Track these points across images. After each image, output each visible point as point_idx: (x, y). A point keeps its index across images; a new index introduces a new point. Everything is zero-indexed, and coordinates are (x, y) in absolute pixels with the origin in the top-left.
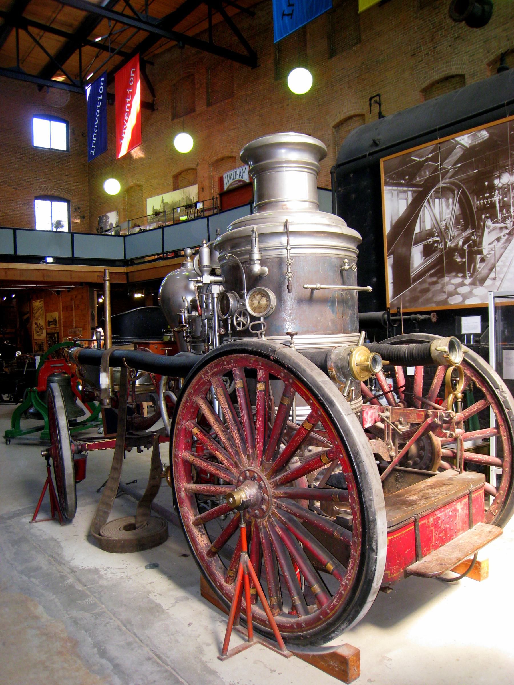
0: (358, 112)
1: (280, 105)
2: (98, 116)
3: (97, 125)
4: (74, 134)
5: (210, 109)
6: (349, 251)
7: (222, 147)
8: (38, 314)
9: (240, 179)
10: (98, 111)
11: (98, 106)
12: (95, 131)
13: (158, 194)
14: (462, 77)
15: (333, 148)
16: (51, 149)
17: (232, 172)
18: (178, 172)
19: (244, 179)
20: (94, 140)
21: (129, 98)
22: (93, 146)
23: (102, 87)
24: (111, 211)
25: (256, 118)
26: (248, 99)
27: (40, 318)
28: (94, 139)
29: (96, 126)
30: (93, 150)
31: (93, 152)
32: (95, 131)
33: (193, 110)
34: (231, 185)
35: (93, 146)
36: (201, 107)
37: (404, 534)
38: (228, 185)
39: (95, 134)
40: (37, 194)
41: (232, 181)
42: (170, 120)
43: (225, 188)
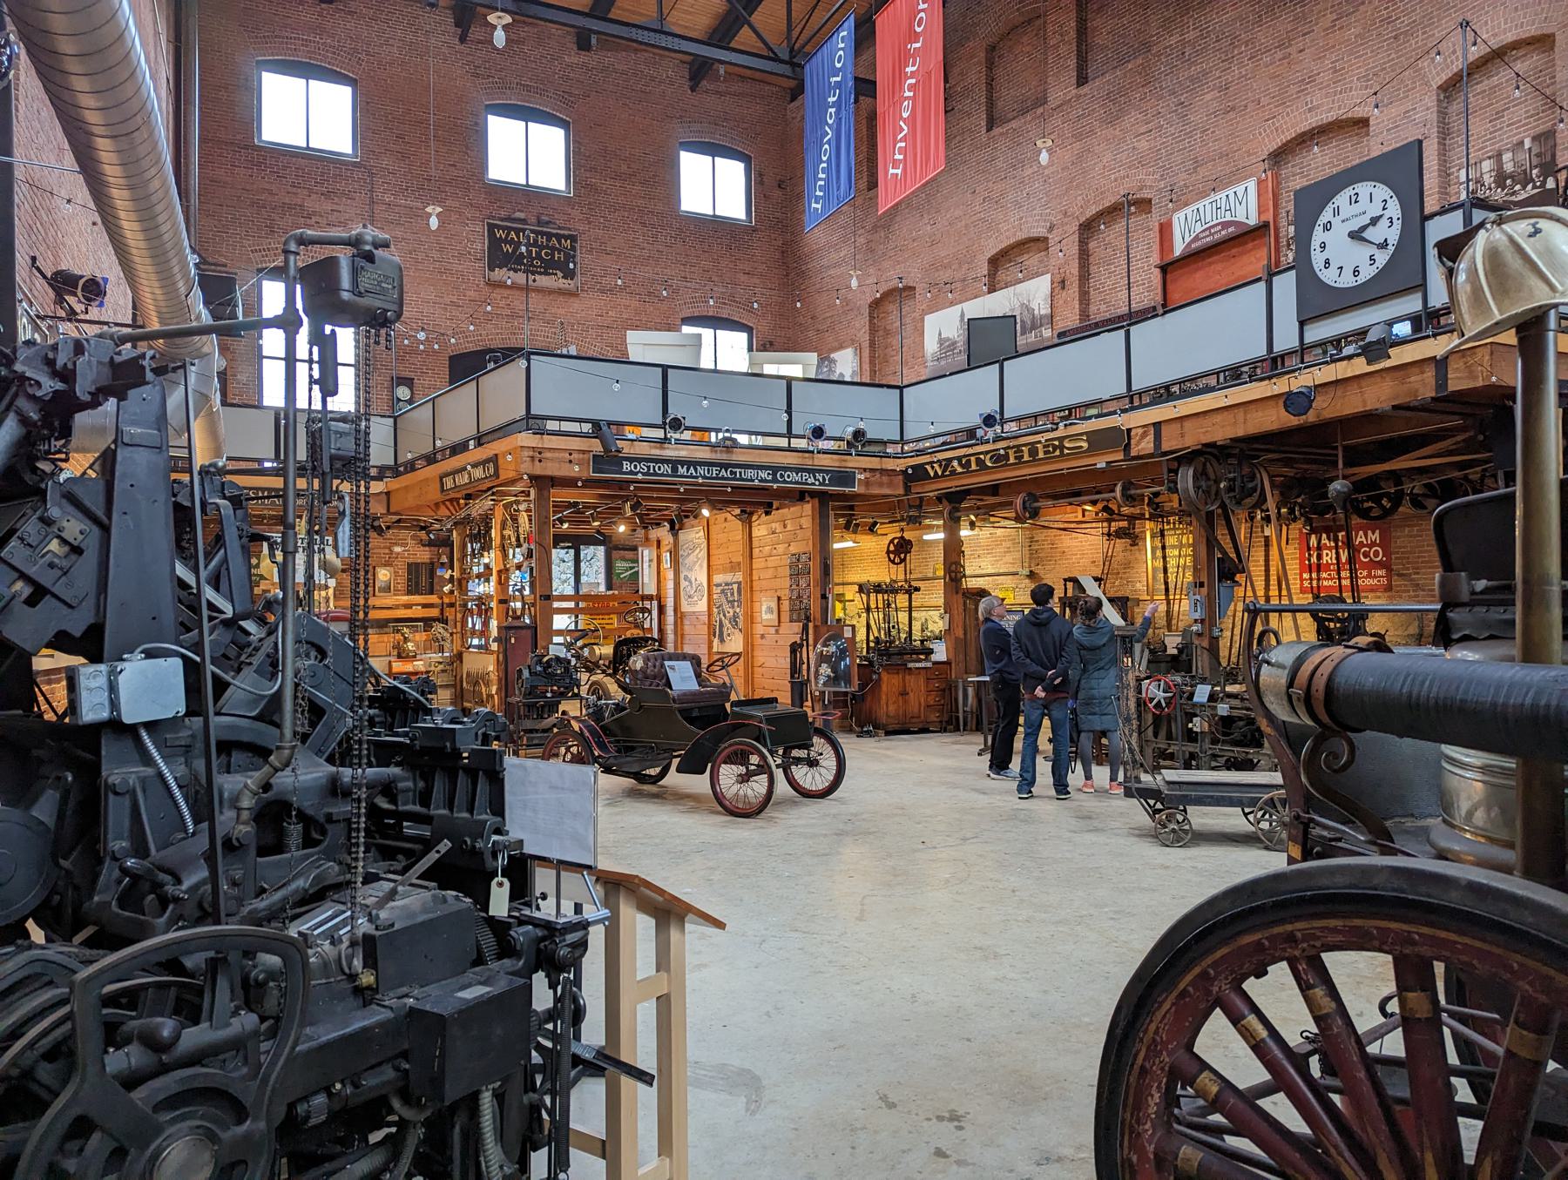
0: (1532, 30)
1: (1279, 55)
2: (830, 122)
3: (829, 142)
4: (760, 182)
5: (1085, 89)
6: (99, 606)
7: (1116, 180)
8: (692, 558)
9: (1228, 218)
10: (832, 110)
11: (831, 100)
12: (824, 159)
13: (952, 304)
14: (1363, 123)
15: (1439, 143)
16: (714, 216)
17: (1201, 206)
18: (1001, 251)
19: (1241, 218)
20: (821, 179)
21: (913, 65)
22: (819, 193)
23: (841, 52)
24: (841, 347)
25: (1208, 97)
26: (1188, 51)
27: (697, 567)
28: (821, 176)
29: (827, 146)
30: (817, 202)
31: (819, 206)
32: (824, 159)
33: (1042, 101)
34: (1196, 239)
35: (819, 193)
36: (1061, 88)
37: (1518, 1012)
38: (1187, 240)
39: (825, 165)
40: (687, 313)
41: (1199, 228)
42: (984, 130)
43: (1179, 249)
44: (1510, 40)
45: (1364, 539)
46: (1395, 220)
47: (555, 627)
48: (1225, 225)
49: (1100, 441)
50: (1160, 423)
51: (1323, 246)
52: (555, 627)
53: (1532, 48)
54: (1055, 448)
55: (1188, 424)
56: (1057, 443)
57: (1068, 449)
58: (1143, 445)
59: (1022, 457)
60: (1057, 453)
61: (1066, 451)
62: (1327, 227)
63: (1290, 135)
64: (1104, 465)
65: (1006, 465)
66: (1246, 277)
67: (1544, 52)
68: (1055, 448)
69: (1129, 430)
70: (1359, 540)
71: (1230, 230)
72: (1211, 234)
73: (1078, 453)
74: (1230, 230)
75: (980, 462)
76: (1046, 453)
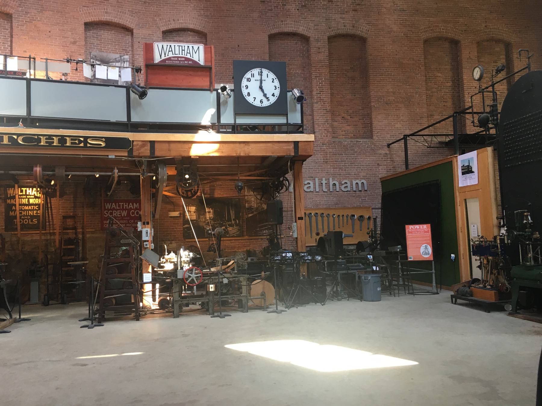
9: (188, 56)
19: (196, 58)
44: (191, 27)
45: (132, 206)
46: (277, 88)
47: (344, 243)
48: (187, 59)
49: (111, 143)
50: (154, 141)
51: (247, 87)
52: (344, 243)
53: (195, 34)
54: (80, 142)
55: (172, 145)
56: (82, 139)
57: (90, 144)
58: (142, 150)
59: (53, 142)
60: (82, 145)
61: (89, 145)
62: (249, 80)
63: (121, 22)
64: (114, 157)
65: (37, 145)
66: (179, 86)
67: (200, 38)
68: (80, 142)
69: (133, 141)
70: (130, 207)
71: (190, 62)
72: (178, 60)
73: (97, 147)
74: (190, 62)
75: (11, 139)
76: (72, 143)
